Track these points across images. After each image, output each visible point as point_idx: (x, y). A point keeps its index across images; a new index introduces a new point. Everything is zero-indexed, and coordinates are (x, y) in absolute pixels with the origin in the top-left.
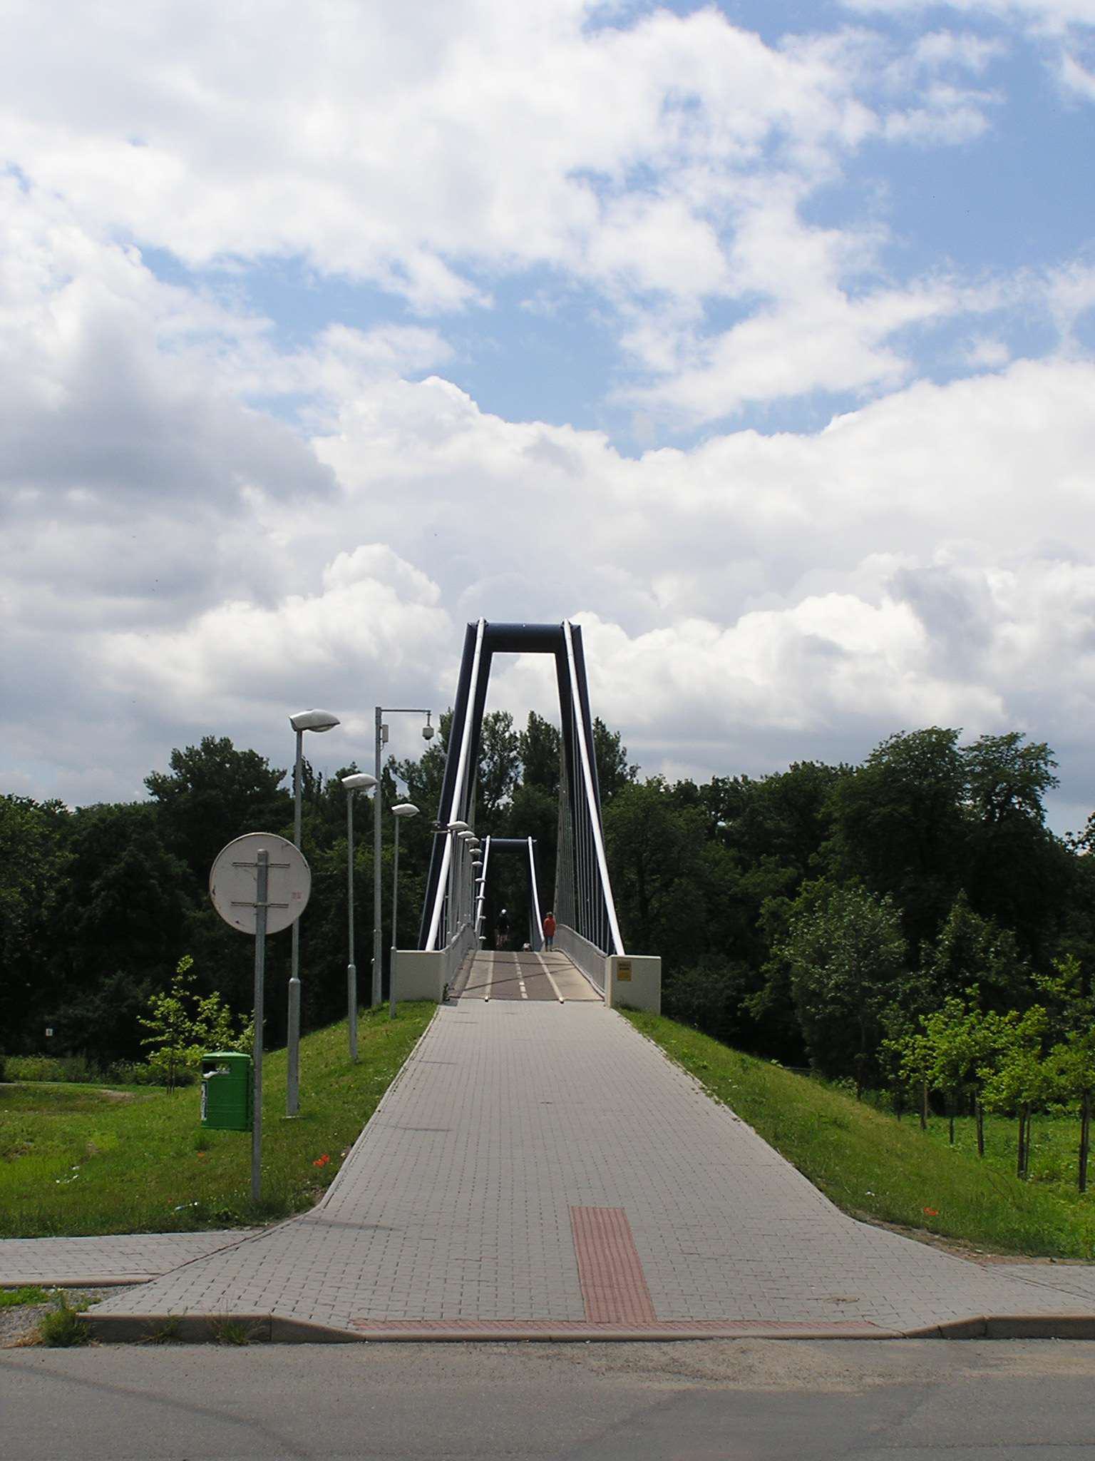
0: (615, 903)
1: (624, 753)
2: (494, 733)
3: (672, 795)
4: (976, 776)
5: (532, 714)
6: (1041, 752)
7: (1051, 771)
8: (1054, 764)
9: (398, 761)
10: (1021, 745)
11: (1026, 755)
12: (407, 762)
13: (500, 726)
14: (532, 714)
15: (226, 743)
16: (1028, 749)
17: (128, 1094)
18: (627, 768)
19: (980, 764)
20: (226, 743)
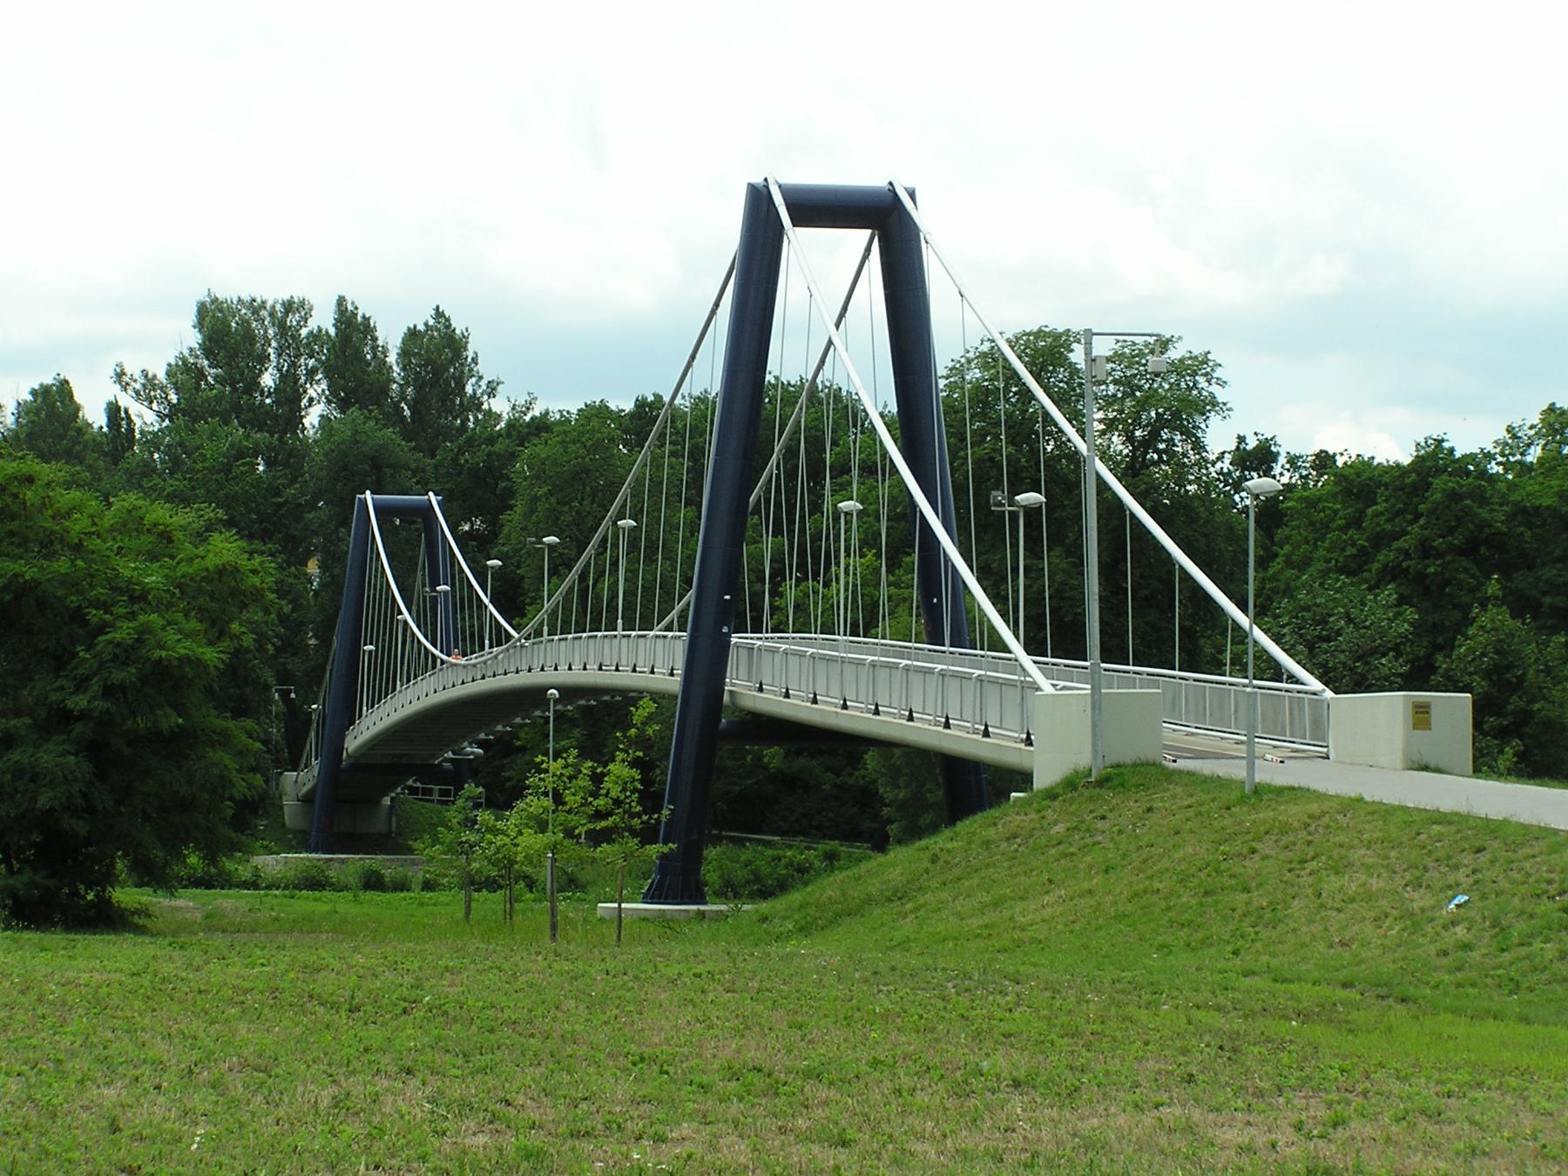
0: (1158, 543)
1: (475, 361)
2: (283, 328)
3: (492, 439)
4: (1110, 401)
5: (341, 301)
6: (1199, 365)
7: (1221, 395)
8: (1222, 383)
9: (128, 371)
10: (1174, 354)
11: (1179, 368)
12: (145, 373)
13: (292, 320)
14: (341, 301)
15: (440, 353)
16: (1181, 360)
17: (723, 907)
18: (483, 383)
19: (1115, 382)
20: (440, 353)
